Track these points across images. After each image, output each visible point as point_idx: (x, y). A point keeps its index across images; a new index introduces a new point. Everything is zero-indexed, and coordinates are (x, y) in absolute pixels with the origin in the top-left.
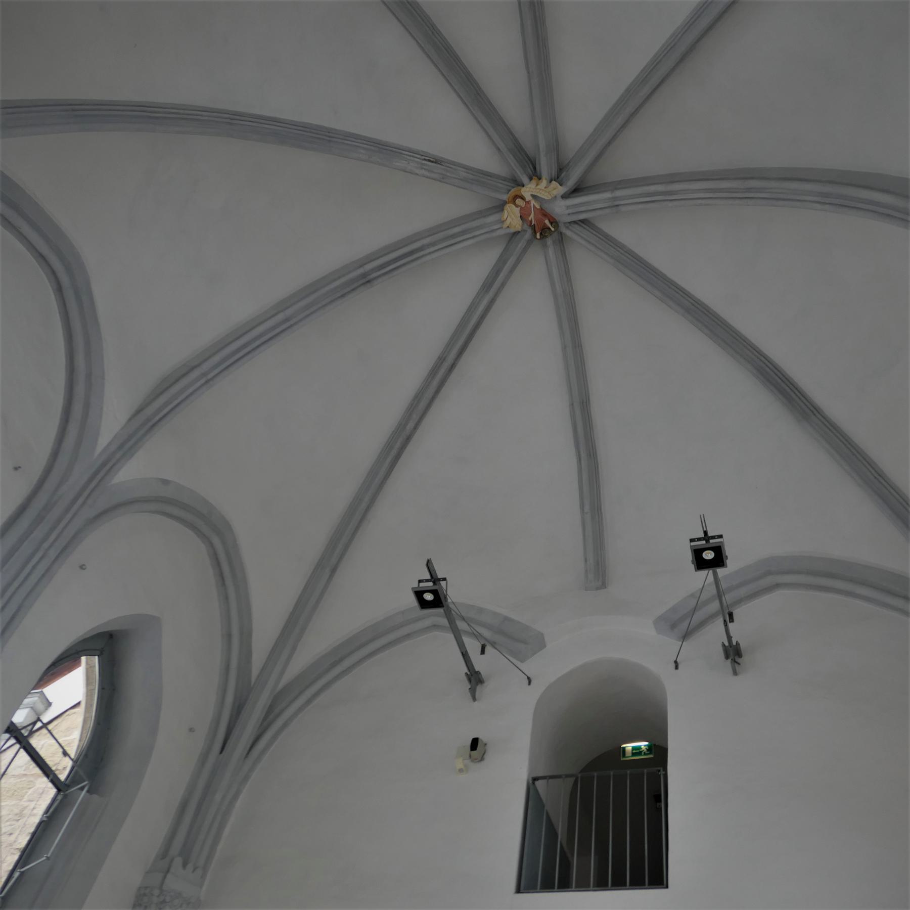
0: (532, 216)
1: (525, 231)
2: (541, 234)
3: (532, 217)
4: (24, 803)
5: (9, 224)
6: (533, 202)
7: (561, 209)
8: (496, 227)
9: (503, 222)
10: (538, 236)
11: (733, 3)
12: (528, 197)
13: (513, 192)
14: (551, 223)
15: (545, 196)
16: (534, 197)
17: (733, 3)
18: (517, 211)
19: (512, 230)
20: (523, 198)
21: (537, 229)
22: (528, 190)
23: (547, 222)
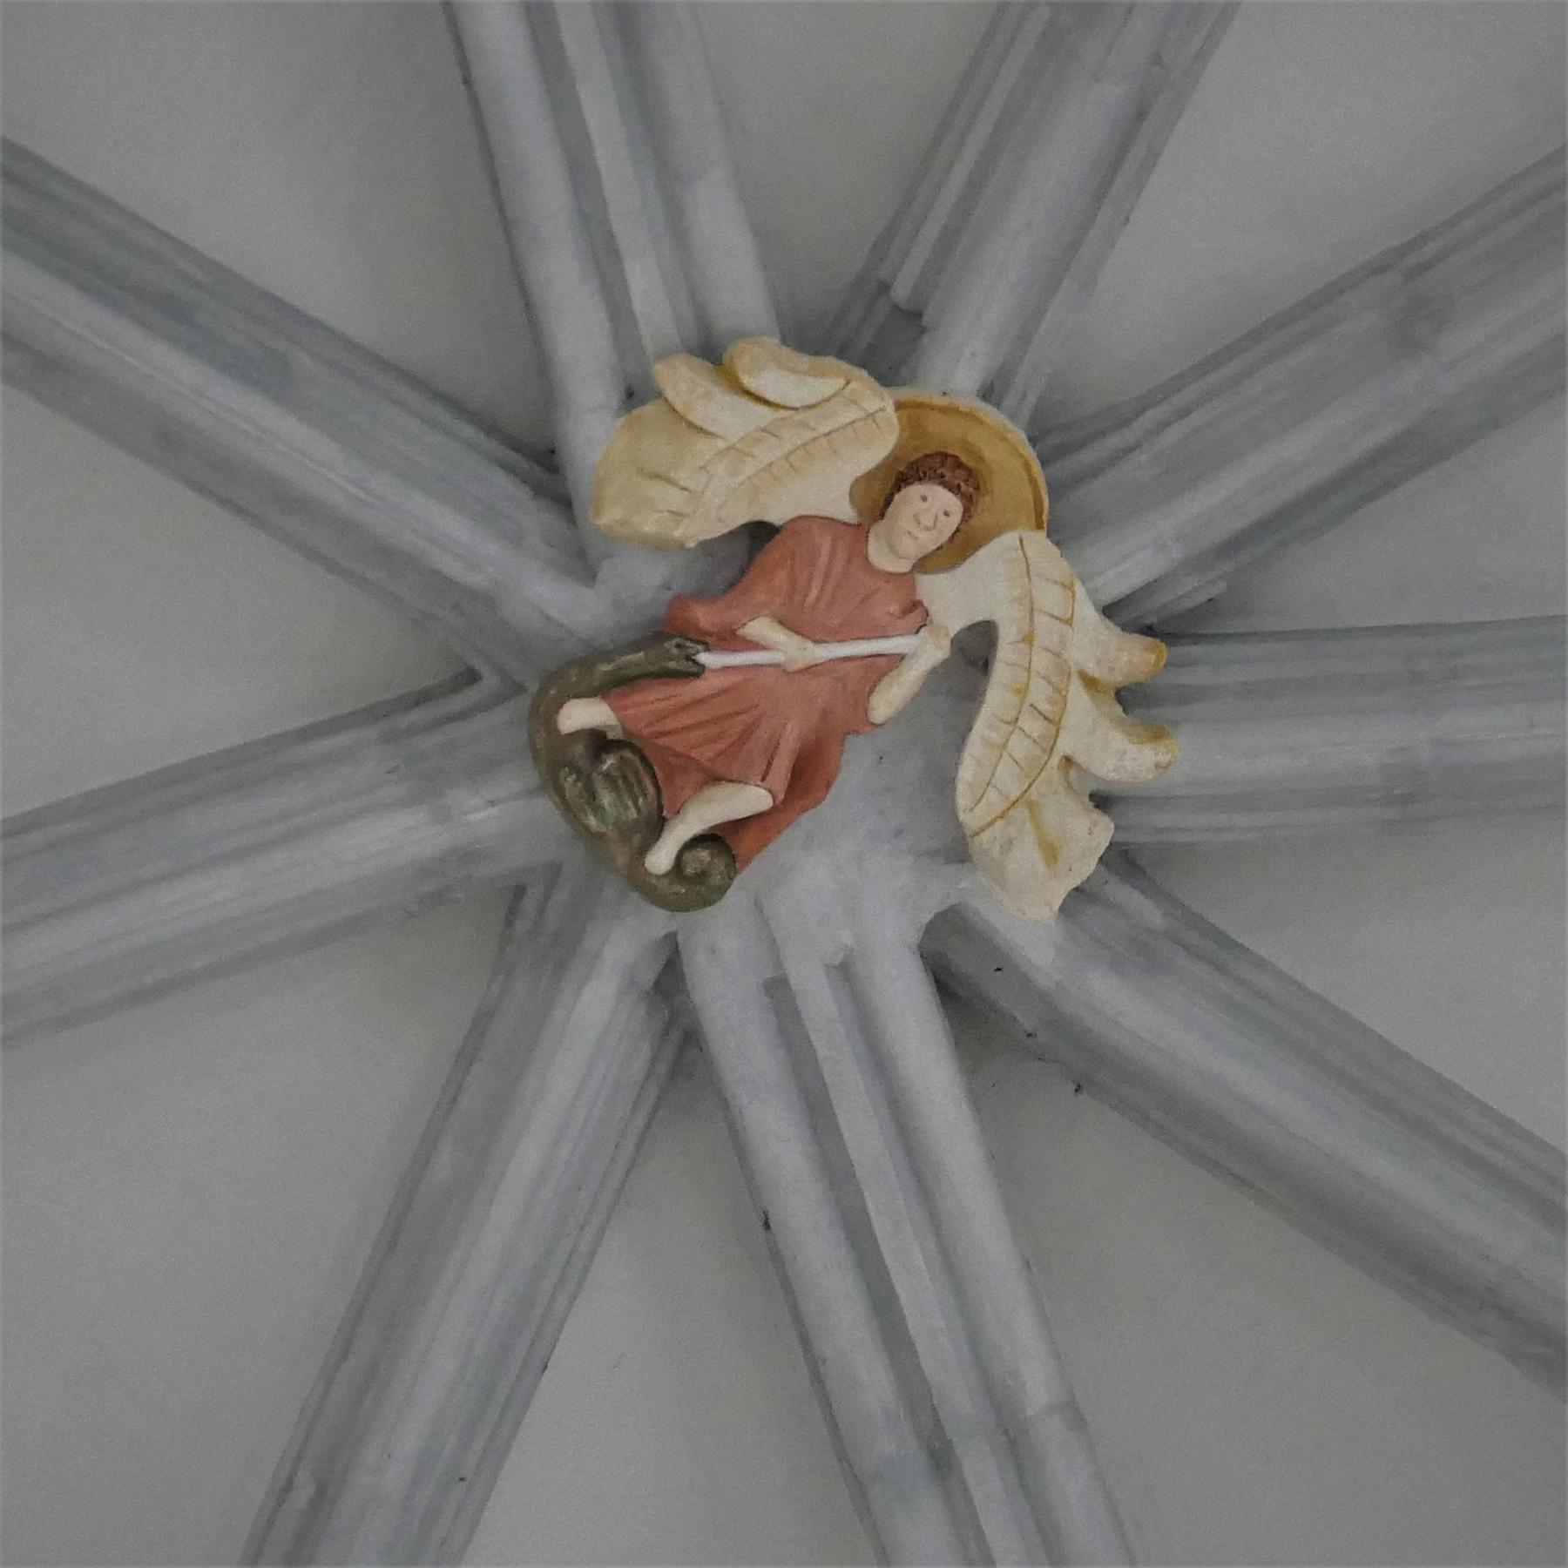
0: (782, 647)
1: (581, 559)
2: (598, 741)
3: (777, 645)
4: (611, 832)
5: (47, 372)
6: (926, 653)
7: (837, 899)
8: (645, 282)
9: (711, 350)
10: (581, 715)
11: (15, 343)
12: (954, 600)
13: (1003, 444)
14: (713, 838)
15: (991, 765)
16: (975, 651)
17: (15, 343)
18: (827, 492)
19: (593, 433)
20: (958, 549)
21: (653, 700)
22: (1017, 584)
23: (751, 799)
